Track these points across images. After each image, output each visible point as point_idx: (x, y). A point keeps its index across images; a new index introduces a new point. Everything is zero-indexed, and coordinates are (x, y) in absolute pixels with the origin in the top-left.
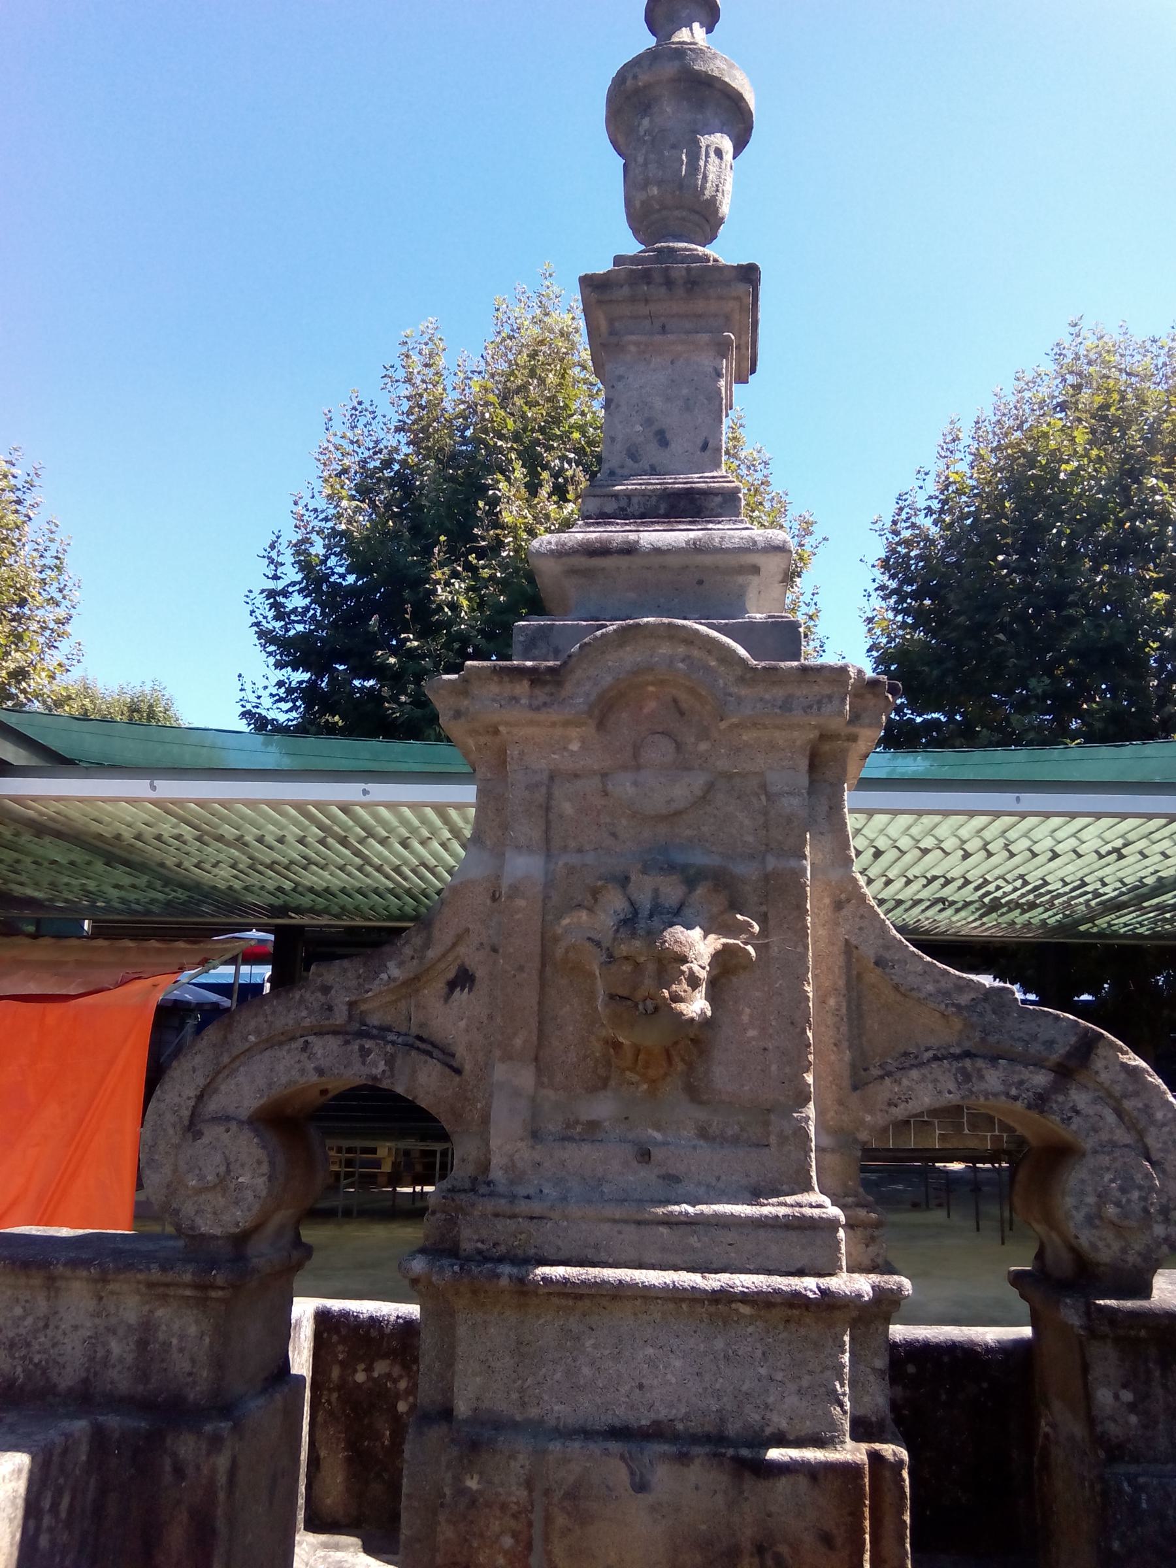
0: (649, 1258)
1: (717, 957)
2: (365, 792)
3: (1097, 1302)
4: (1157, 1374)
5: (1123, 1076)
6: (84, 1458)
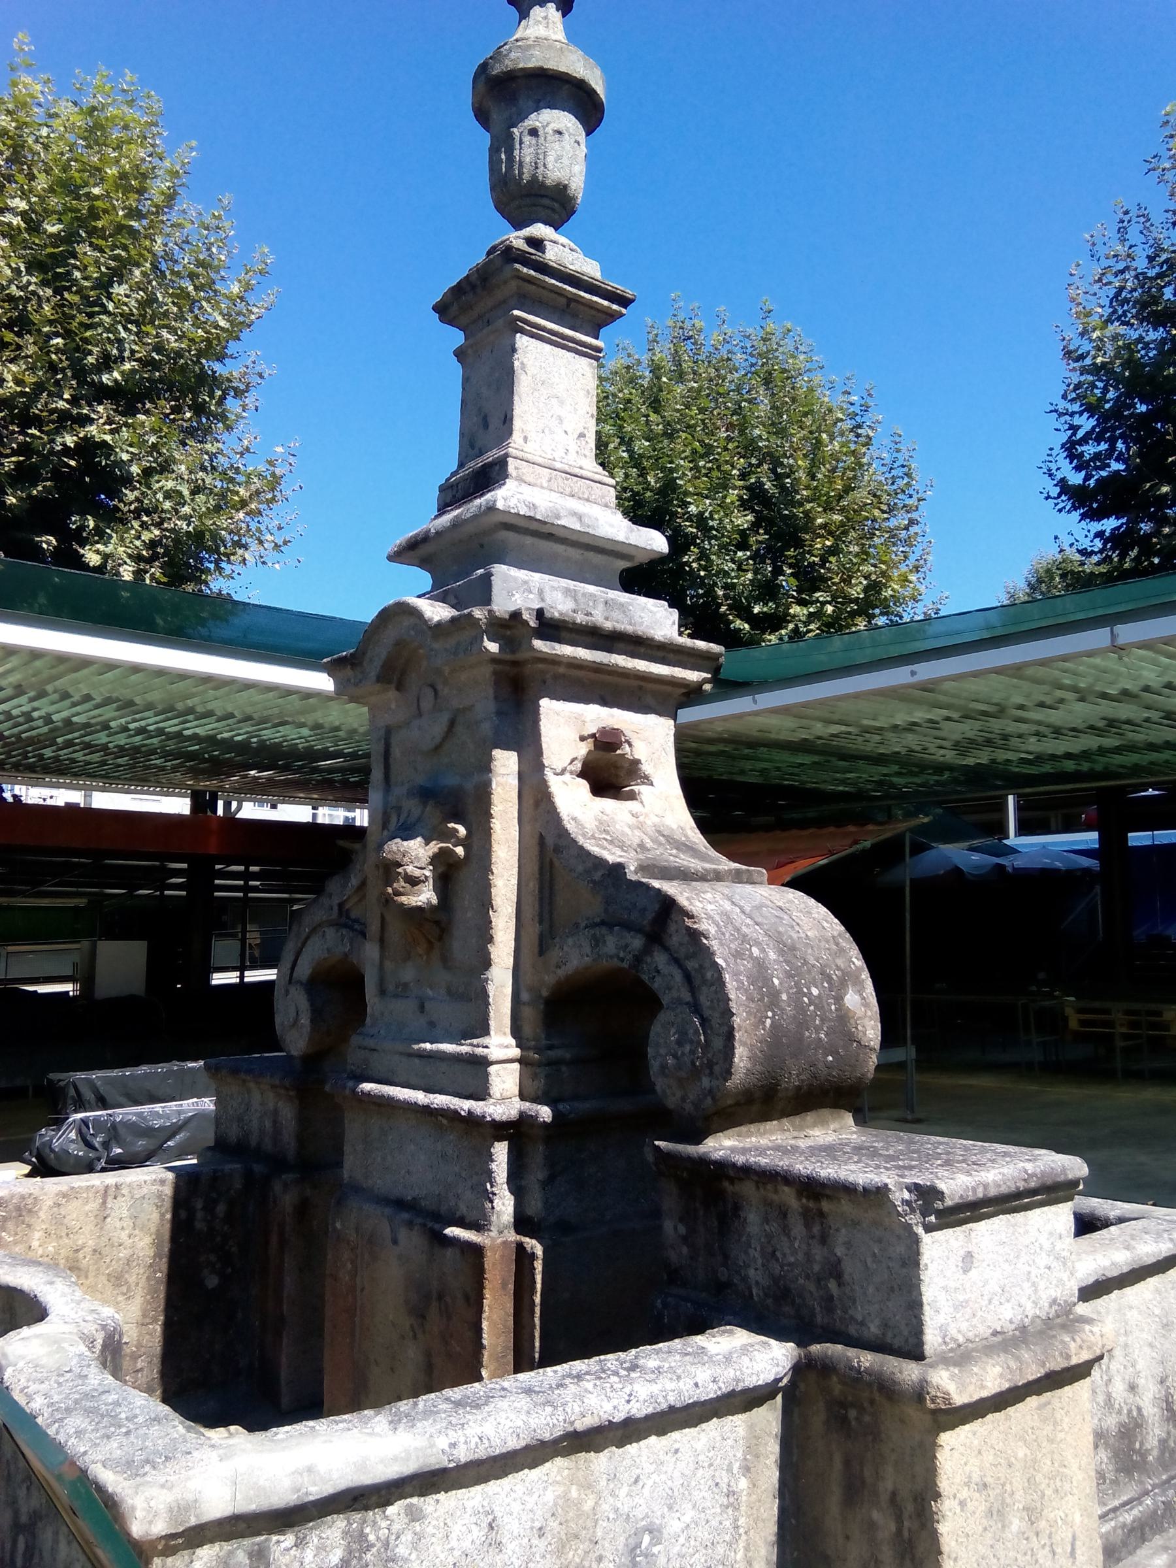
0: (413, 1082)
1: (435, 860)
2: (913, 673)
3: (656, 1143)
4: (701, 1213)
5: (687, 938)
6: (238, 1186)
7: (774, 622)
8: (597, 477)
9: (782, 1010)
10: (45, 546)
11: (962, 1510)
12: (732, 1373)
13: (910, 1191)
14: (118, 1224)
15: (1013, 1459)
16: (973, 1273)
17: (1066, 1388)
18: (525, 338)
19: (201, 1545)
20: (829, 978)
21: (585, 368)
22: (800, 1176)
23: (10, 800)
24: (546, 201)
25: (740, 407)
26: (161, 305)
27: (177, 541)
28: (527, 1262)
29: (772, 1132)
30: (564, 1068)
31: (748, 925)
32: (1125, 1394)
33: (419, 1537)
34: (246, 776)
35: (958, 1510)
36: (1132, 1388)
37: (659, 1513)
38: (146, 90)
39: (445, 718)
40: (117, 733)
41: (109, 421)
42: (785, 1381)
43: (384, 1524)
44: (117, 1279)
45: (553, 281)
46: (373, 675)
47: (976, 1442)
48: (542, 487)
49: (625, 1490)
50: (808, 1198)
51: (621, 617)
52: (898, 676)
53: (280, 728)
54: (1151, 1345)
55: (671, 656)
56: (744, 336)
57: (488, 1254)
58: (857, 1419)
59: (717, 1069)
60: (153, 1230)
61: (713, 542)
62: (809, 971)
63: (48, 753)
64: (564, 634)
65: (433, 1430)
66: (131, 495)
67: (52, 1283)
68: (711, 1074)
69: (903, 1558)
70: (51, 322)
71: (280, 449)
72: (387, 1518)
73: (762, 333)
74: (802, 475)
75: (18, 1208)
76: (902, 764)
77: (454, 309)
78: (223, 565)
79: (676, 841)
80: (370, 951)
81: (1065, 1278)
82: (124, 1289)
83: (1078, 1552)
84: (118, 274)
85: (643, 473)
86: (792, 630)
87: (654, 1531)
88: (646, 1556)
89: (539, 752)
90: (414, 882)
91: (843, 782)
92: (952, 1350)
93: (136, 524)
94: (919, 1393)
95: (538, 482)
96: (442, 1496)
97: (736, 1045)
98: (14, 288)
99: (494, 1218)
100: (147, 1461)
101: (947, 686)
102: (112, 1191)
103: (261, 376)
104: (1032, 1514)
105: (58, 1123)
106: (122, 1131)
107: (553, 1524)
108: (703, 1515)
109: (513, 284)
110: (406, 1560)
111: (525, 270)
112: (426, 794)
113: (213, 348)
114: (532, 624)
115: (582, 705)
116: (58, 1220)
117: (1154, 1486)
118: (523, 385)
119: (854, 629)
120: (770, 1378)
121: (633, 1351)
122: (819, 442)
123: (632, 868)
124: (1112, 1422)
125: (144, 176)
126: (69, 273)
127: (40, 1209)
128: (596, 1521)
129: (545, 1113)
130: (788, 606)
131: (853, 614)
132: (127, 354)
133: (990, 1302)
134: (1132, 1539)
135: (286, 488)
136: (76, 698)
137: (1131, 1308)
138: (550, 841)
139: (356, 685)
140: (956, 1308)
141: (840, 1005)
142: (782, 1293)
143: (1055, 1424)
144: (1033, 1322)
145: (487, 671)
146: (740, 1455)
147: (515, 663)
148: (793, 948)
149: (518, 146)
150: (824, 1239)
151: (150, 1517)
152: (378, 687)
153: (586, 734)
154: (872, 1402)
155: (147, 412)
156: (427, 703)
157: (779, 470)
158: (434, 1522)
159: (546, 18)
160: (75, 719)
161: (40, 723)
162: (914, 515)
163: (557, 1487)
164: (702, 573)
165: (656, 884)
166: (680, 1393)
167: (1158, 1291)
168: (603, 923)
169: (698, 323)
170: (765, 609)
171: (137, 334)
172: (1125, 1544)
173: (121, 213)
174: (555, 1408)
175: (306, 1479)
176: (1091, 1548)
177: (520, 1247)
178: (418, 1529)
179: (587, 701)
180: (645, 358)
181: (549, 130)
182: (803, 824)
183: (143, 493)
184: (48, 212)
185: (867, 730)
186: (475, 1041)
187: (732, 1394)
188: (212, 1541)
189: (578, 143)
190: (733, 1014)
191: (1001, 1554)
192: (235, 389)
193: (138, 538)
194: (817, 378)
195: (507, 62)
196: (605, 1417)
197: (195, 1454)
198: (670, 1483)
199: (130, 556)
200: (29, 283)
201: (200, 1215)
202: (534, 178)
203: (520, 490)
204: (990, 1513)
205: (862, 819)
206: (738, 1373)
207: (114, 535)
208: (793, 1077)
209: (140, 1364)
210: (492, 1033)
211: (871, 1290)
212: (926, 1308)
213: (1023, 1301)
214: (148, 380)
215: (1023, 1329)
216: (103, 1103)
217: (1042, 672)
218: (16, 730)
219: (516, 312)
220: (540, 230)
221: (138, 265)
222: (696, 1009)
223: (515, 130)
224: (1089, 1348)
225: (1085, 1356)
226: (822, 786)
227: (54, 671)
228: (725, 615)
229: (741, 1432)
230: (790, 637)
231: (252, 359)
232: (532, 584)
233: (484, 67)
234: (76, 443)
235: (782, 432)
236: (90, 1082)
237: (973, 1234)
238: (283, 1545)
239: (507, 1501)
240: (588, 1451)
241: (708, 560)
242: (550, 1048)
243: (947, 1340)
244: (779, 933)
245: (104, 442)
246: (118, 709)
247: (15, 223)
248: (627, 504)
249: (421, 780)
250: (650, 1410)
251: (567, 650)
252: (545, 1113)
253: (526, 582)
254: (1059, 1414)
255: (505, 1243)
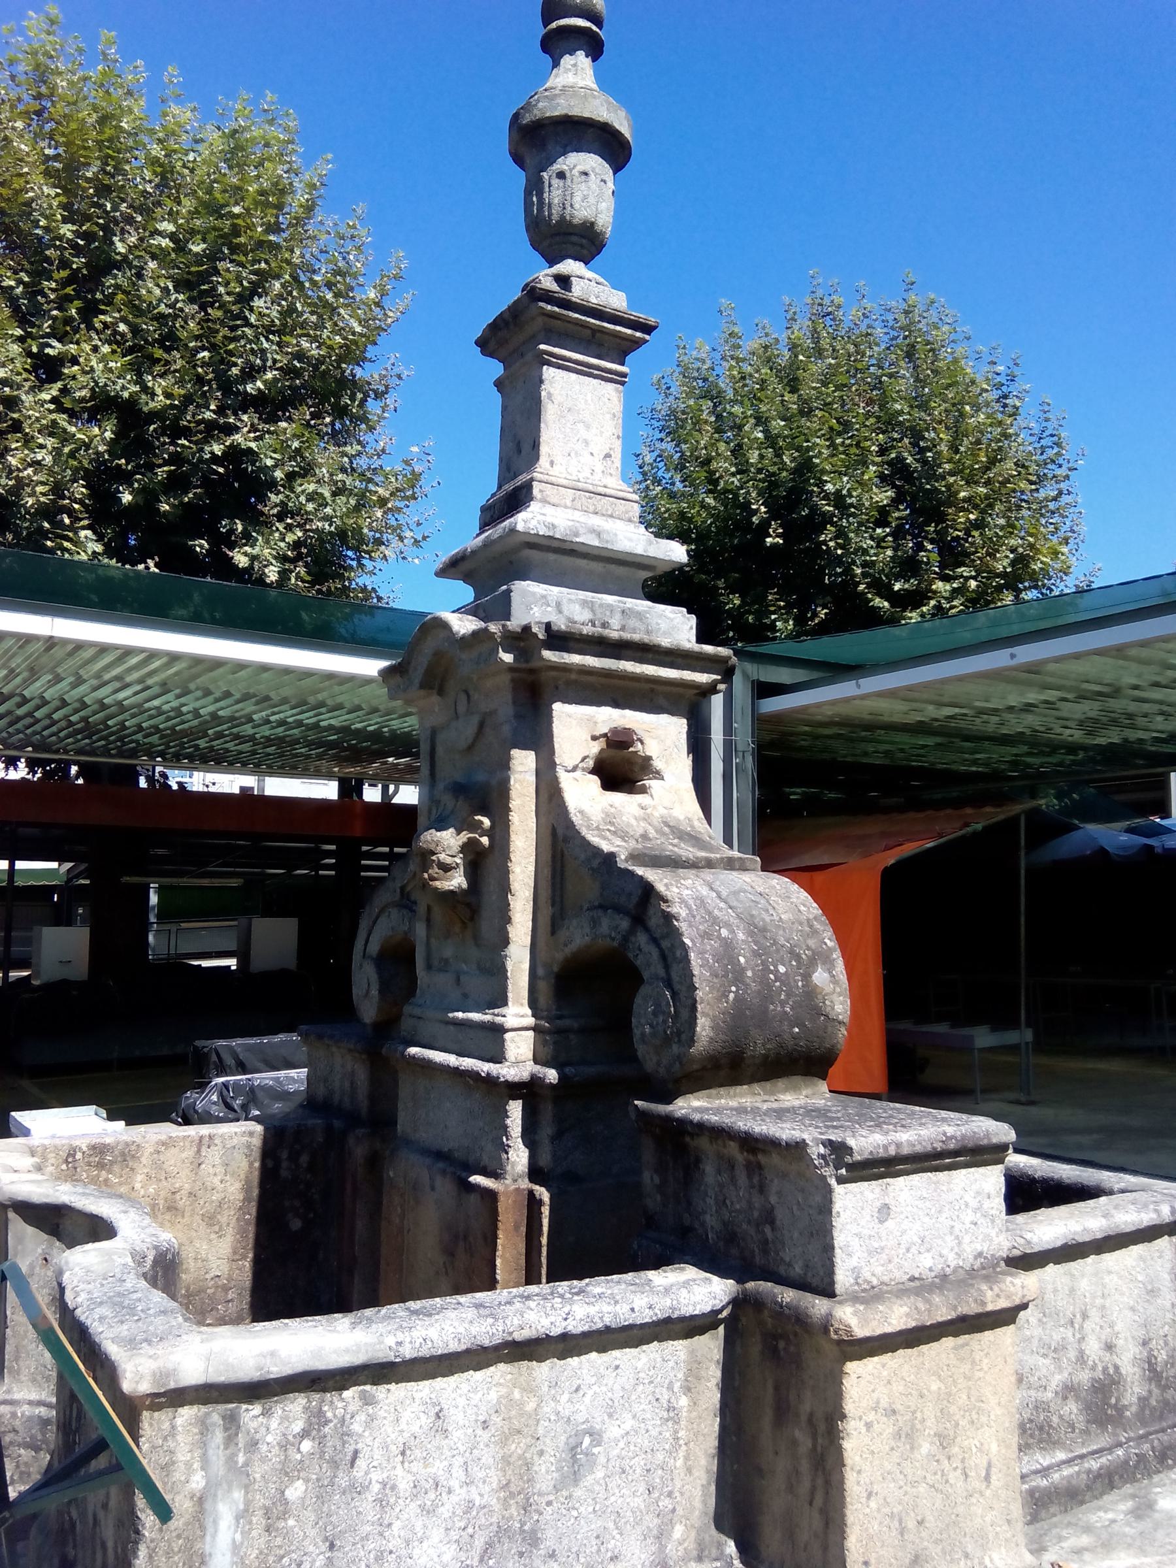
1: (467, 848)
2: (1013, 656)
3: (636, 1102)
6: (321, 1140)
7: (915, 599)
8: (621, 494)
9: (747, 985)
10: (198, 549)
11: (868, 1430)
12: (668, 1303)
13: (825, 1146)
14: (211, 1171)
15: (925, 1392)
16: (890, 1224)
17: (987, 1333)
18: (552, 370)
19: (182, 1405)
20: (798, 957)
21: (610, 390)
22: (739, 1132)
23: (175, 787)
24: (574, 239)
25: (880, 382)
26: (301, 314)
27: (321, 540)
28: (536, 1207)
29: (741, 1096)
30: (572, 1036)
31: (720, 909)
32: (1101, 1353)
33: (372, 1418)
34: (386, 763)
35: (864, 1430)
36: (1109, 1347)
37: (599, 1420)
38: (285, 109)
39: (475, 720)
40: (260, 725)
41: (253, 428)
42: (725, 1314)
43: (340, 1404)
44: (210, 1219)
45: (576, 315)
46: (417, 681)
47: (885, 1373)
48: (566, 507)
49: (566, 1397)
50: (748, 1151)
51: (638, 624)
52: (998, 659)
53: (407, 719)
54: (1133, 1309)
55: (680, 660)
56: (886, 310)
57: (502, 1199)
58: (785, 1349)
59: (684, 1037)
60: (243, 1176)
61: (851, 519)
62: (778, 951)
63: (202, 743)
64: (571, 644)
65: (384, 1331)
66: (274, 498)
67: (126, 1212)
68: (679, 1041)
69: (817, 1470)
70: (197, 338)
71: (415, 449)
72: (343, 1400)
73: (904, 306)
74: (943, 448)
75: (123, 1154)
76: (1033, 745)
77: (492, 345)
78: (364, 562)
79: (681, 831)
80: (420, 930)
81: (993, 1234)
82: (216, 1228)
83: (994, 1478)
84: (255, 290)
85: (778, 454)
86: (935, 606)
87: (596, 1436)
88: (587, 1455)
89: (552, 752)
90: (446, 868)
91: (975, 762)
92: (864, 1291)
93: (281, 526)
94: (825, 1326)
95: (563, 502)
96: (393, 1386)
97: (699, 1015)
98: (163, 306)
99: (509, 1168)
100: (146, 1340)
101: (1051, 667)
102: (206, 1141)
103: (399, 377)
104: (944, 1441)
105: (202, 1086)
106: (260, 1095)
107: (496, 1420)
108: (642, 1425)
109: (540, 321)
110: (360, 1436)
111: (549, 307)
112: (460, 789)
113: (352, 352)
114: (541, 636)
115: (594, 708)
116: (158, 1166)
117: (1129, 1440)
118: (550, 413)
119: (999, 604)
120: (707, 1308)
121: (587, 1280)
122: (962, 414)
123: (623, 857)
124: (1084, 1377)
125: (283, 192)
126: (214, 289)
127: (142, 1155)
128: (538, 1421)
129: (552, 1075)
130: (931, 582)
131: (999, 589)
132: (269, 363)
133: (908, 1250)
134: (1098, 1485)
135: (426, 484)
136: (218, 694)
137: (1110, 1272)
138: (560, 832)
139: (405, 691)
140: (870, 1253)
141: (807, 981)
142: (731, 1236)
143: (973, 1362)
144: (955, 1271)
145: (505, 679)
146: (680, 1375)
147: (532, 671)
148: (764, 930)
149: (547, 189)
150: (762, 1189)
151: (137, 1379)
152: (422, 692)
153: (597, 734)
154: (796, 1334)
155: (290, 420)
156: (462, 708)
157: (921, 443)
158: (386, 1408)
159: (575, 65)
160: (221, 713)
161: (189, 716)
162: (1062, 485)
163: (500, 1388)
164: (839, 552)
165: (640, 871)
166: (615, 1316)
167: (1141, 1258)
168: (601, 906)
169: (837, 299)
170: (906, 586)
171: (279, 344)
172: (1089, 1488)
173: (259, 229)
174: (497, 1320)
175: (268, 1361)
176: (1008, 1475)
177: (531, 1193)
178: (371, 1411)
179: (598, 703)
180: (783, 337)
181: (575, 172)
182: (938, 805)
183: (287, 496)
184: (193, 232)
185: (981, 712)
186: (496, 1011)
187: (668, 1321)
188: (191, 1403)
189: (605, 182)
190: (696, 989)
191: (909, 1471)
192: (376, 392)
193: (283, 540)
194: (960, 350)
195: (536, 112)
196: (543, 1330)
197: (184, 1337)
198: (610, 1394)
199: (275, 558)
200: (177, 301)
201: (285, 1164)
202: (562, 217)
203: (543, 511)
204: (898, 1435)
205: (979, 801)
206: (675, 1302)
207: (260, 538)
208: (758, 1045)
209: (230, 1295)
210: (510, 1004)
211: (796, 1235)
212: (838, 1251)
213: (945, 1252)
214: (290, 387)
215: (944, 1277)
216: (242, 1068)
217: (1145, 653)
218: (170, 723)
219: (542, 347)
220: (569, 266)
221: (278, 277)
222: (669, 984)
223: (544, 174)
224: (1008, 1297)
225: (1003, 1304)
226: (954, 767)
227: (193, 671)
228: (863, 593)
229: (683, 1355)
230: (933, 615)
231: (392, 361)
232: (549, 598)
233: (516, 117)
234: (224, 453)
235: (924, 406)
236: (230, 1048)
237: (890, 1189)
238: (252, 1413)
239: (454, 1395)
240: (530, 1360)
241: (848, 540)
242: (560, 1017)
243: (860, 1281)
244: (752, 916)
245: (250, 449)
246: (257, 703)
247: (164, 245)
248: (761, 485)
249: (459, 777)
250: (586, 1328)
251: (576, 659)
252: (552, 1075)
253: (544, 597)
254: (978, 1356)
255: (517, 1190)
